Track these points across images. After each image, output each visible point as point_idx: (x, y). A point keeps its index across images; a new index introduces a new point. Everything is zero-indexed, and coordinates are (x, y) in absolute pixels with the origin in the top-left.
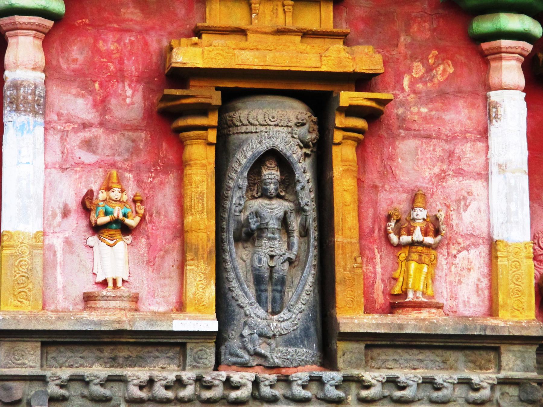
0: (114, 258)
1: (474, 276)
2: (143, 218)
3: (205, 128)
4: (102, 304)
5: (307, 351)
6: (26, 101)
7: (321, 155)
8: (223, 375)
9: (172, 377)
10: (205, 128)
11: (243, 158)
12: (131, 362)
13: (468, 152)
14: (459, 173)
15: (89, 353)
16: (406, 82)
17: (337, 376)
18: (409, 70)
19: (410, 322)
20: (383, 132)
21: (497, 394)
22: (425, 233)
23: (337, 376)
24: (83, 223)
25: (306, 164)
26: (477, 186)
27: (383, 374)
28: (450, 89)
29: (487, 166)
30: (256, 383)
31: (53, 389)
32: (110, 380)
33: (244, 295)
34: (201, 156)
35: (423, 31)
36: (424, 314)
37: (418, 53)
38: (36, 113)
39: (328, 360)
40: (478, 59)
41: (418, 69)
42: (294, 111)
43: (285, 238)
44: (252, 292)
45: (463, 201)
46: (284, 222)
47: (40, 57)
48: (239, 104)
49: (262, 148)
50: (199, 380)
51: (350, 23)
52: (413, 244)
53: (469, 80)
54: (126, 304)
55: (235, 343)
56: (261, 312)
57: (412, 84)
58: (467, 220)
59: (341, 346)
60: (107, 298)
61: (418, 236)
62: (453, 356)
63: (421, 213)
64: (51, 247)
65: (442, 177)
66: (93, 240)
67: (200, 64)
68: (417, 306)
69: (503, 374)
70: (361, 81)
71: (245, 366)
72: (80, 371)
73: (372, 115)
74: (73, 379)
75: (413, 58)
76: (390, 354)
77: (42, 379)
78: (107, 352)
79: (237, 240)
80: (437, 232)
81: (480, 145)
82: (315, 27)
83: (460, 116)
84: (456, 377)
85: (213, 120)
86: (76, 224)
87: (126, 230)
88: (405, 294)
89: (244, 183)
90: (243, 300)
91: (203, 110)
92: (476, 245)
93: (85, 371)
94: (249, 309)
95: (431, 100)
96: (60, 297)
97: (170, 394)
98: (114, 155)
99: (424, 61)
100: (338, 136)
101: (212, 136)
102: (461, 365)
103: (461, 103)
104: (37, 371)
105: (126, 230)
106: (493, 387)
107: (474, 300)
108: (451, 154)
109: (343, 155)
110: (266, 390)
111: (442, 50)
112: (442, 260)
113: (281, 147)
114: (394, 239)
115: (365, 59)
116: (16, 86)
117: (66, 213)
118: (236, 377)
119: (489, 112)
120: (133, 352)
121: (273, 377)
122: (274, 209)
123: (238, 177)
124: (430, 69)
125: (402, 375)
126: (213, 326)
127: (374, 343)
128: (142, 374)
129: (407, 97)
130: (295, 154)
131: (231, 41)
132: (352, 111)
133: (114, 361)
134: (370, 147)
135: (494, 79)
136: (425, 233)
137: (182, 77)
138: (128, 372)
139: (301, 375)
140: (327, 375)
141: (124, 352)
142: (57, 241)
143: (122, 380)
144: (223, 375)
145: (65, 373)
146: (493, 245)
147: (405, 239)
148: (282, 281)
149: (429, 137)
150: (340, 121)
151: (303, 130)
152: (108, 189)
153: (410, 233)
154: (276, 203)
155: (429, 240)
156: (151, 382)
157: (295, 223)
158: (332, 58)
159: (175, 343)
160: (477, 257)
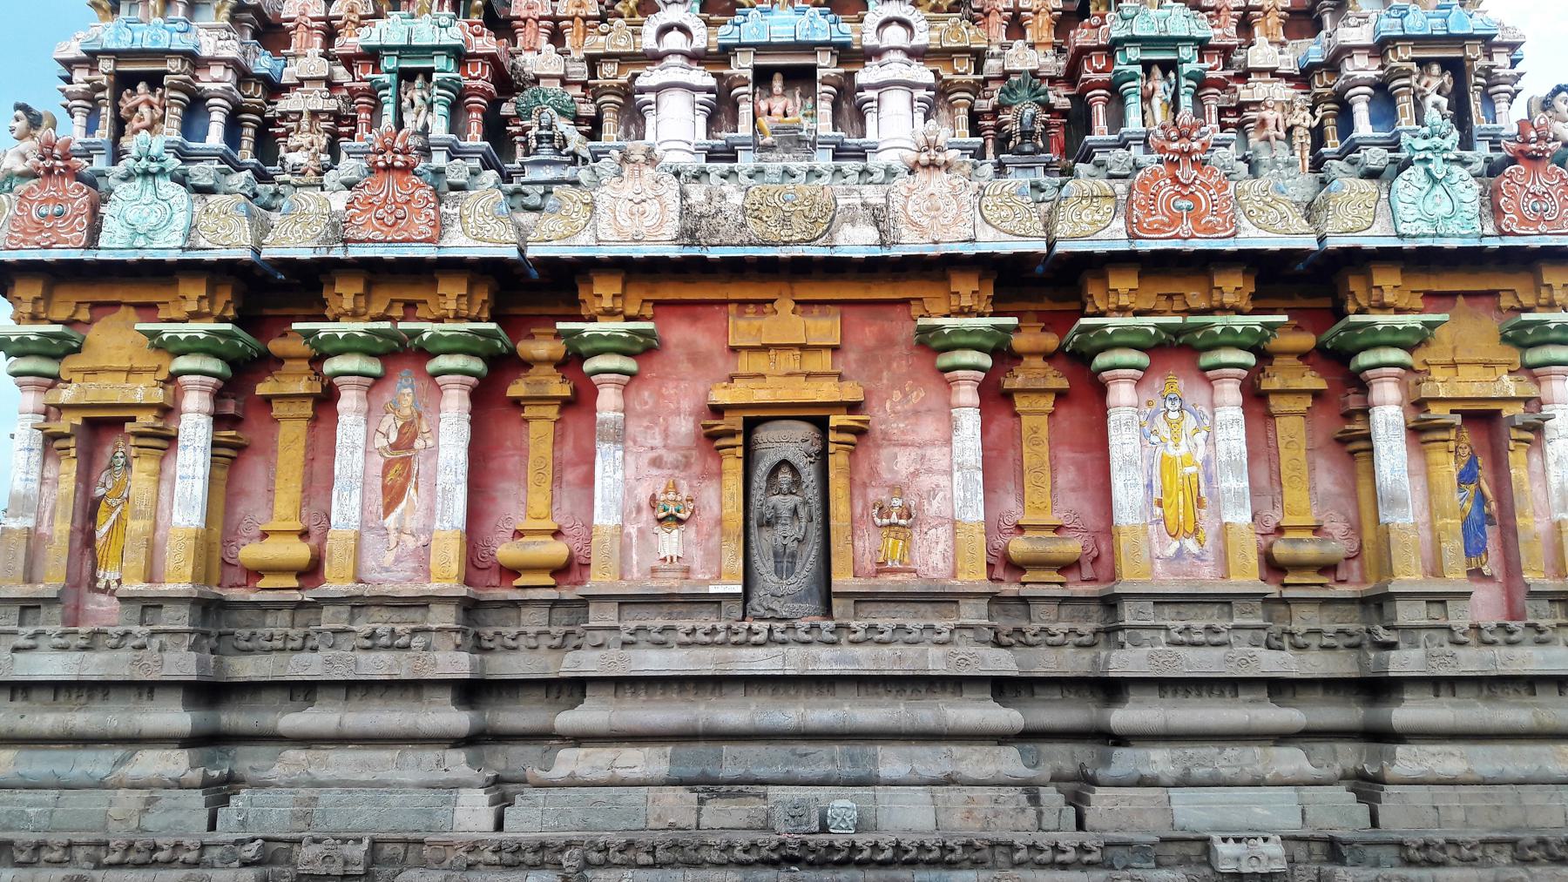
0: (670, 542)
1: (941, 547)
2: (693, 512)
3: (734, 447)
4: (661, 574)
5: (813, 605)
6: (608, 434)
7: (823, 458)
8: (747, 624)
9: (709, 626)
10: (734, 447)
11: (762, 468)
12: (680, 616)
13: (937, 455)
14: (930, 471)
15: (653, 609)
16: (888, 405)
17: (831, 624)
18: (890, 397)
19: (887, 583)
20: (870, 444)
21: (956, 637)
22: (900, 517)
23: (831, 624)
24: (651, 517)
25: (811, 468)
26: (943, 481)
27: (866, 623)
28: (922, 409)
29: (951, 466)
30: (770, 630)
31: (625, 636)
32: (664, 629)
33: (764, 567)
34: (733, 465)
35: (900, 366)
36: (899, 577)
37: (897, 383)
38: (615, 442)
39: (828, 613)
40: (944, 386)
41: (897, 396)
42: (805, 430)
43: (493, 615)
44: (771, 563)
45: (932, 493)
46: (795, 511)
47: (620, 402)
48: (760, 428)
49: (777, 459)
50: (729, 628)
51: (846, 364)
52: (891, 525)
53: (935, 401)
54: (679, 575)
55: (754, 602)
56: (775, 579)
57: (892, 407)
58: (934, 507)
59: (835, 601)
60: (665, 571)
61: (894, 519)
62: (923, 608)
63: (897, 502)
64: (629, 535)
65: (916, 474)
66: (657, 529)
67: (728, 402)
68: (893, 571)
69: (961, 621)
70: (852, 407)
71: (762, 619)
72: (643, 623)
73: (860, 432)
74: (638, 629)
75: (893, 388)
76: (872, 608)
77: (617, 629)
78: (666, 608)
79: (760, 526)
80: (910, 516)
81: (946, 450)
82: (818, 369)
83: (928, 429)
84: (922, 624)
85: (739, 440)
86: (646, 516)
87: (680, 521)
88: (885, 563)
89: (764, 485)
90: (763, 570)
91: (731, 434)
92: (942, 525)
93: (648, 623)
94: (766, 577)
95: (907, 418)
96: (635, 570)
97: (707, 639)
98: (1495, 146)
99: (902, 390)
100: (832, 448)
101: (740, 452)
102: (929, 615)
103: (930, 419)
104: (616, 624)
105: (680, 521)
106: (952, 631)
107: (941, 565)
108: (923, 457)
109: (838, 460)
110: (778, 636)
111: (915, 380)
112: (916, 536)
113: (790, 458)
114: (878, 521)
115: (850, 393)
116: (603, 423)
117: (639, 510)
118: (756, 625)
119: (951, 425)
120: (684, 609)
121: (782, 625)
122: (784, 503)
123: (759, 480)
124: (905, 395)
125: (880, 623)
126: (739, 589)
127: (861, 599)
128: (688, 625)
129: (885, 415)
130: (801, 462)
131: (752, 383)
132: (840, 429)
133: (670, 616)
134: (860, 454)
135: (954, 401)
136: (900, 517)
137: (718, 411)
138: (677, 623)
139: (804, 624)
140: (823, 624)
141: (678, 609)
142: (632, 530)
143: (673, 629)
144: (747, 624)
145: (633, 625)
146: (954, 523)
147: (886, 521)
148: (793, 555)
149: (905, 445)
150: (833, 436)
151: (805, 445)
152: (666, 492)
153: (889, 517)
154: (789, 497)
155: (903, 522)
156: (694, 630)
157: (803, 513)
158: (825, 391)
159: (716, 601)
160: (943, 533)
